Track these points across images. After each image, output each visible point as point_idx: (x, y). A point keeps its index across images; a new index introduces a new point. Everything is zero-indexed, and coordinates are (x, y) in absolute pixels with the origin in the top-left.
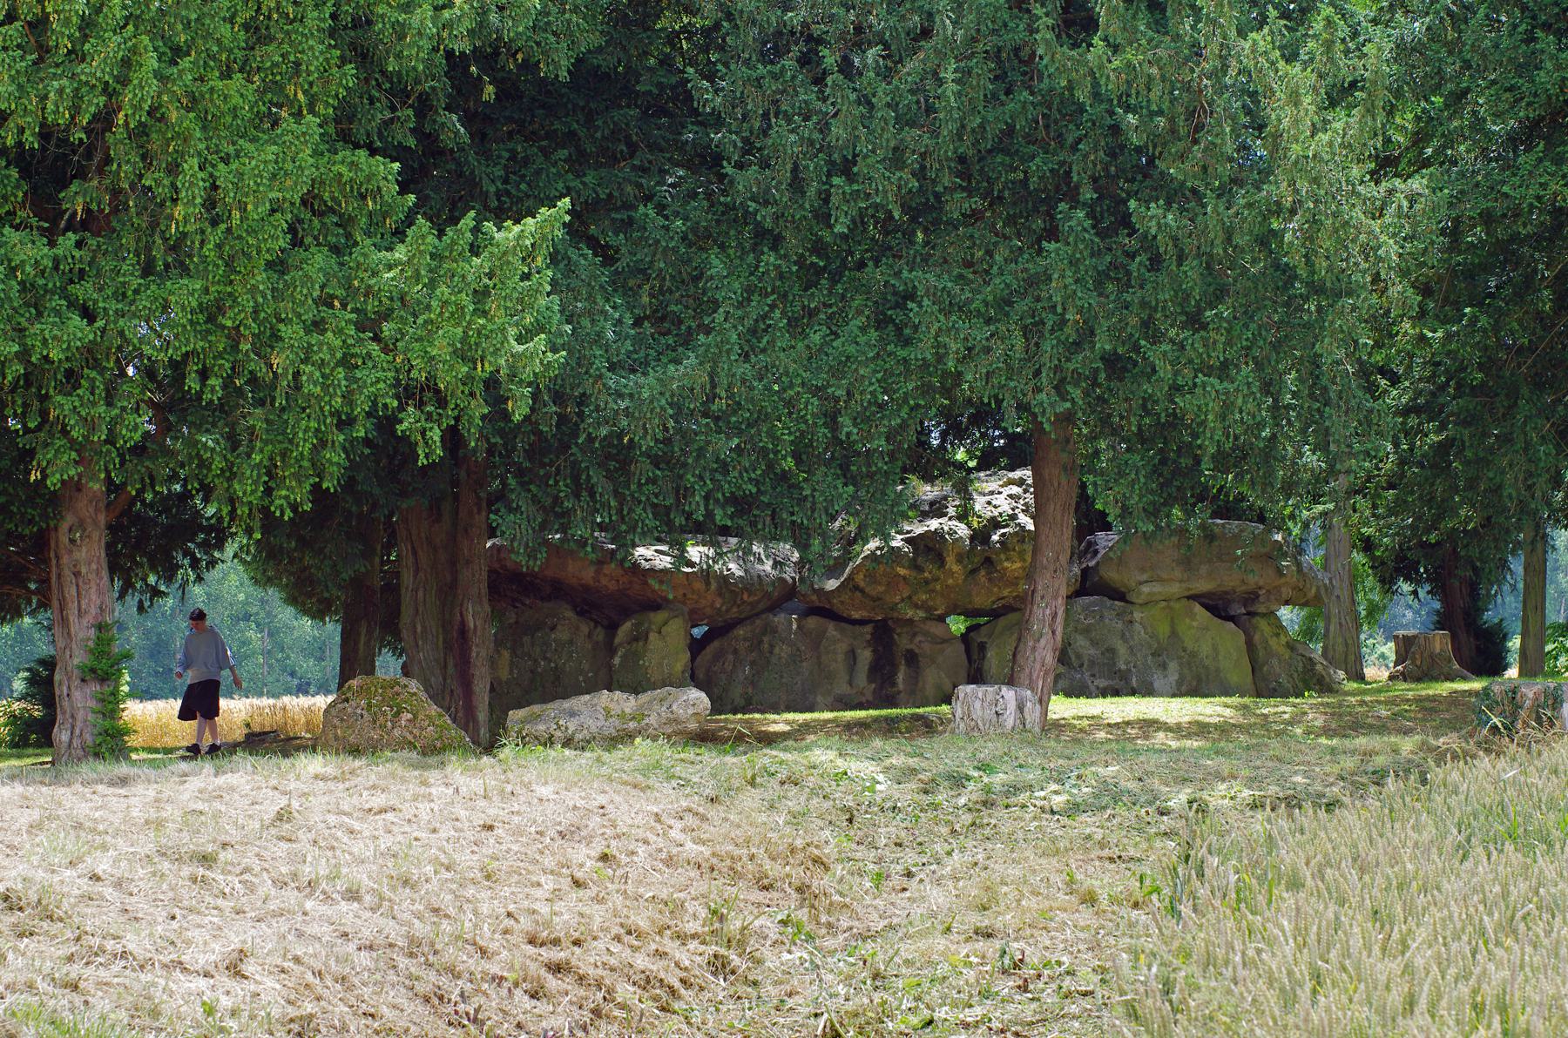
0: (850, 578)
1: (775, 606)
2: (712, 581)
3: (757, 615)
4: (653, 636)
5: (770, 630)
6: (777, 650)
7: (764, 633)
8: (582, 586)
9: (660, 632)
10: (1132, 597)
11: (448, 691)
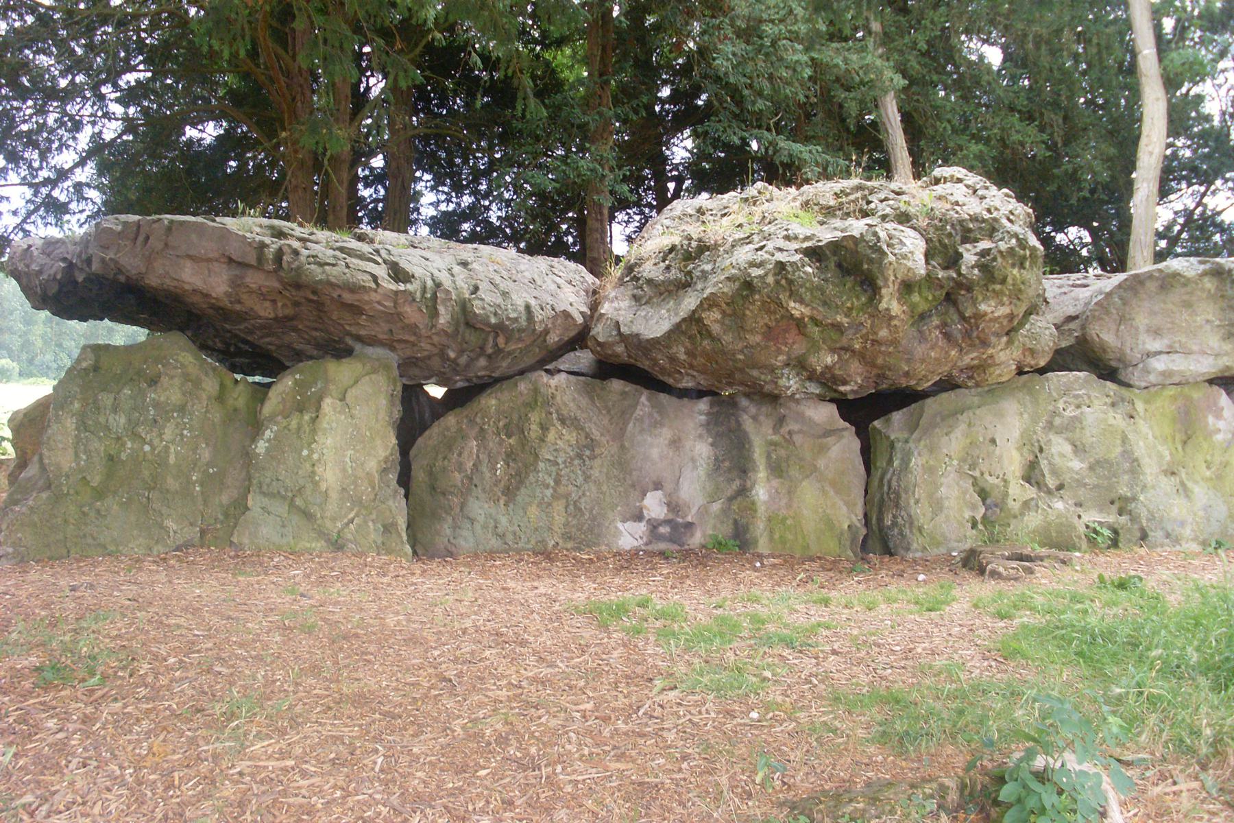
0: (694, 319)
1: (548, 358)
2: (441, 309)
3: (522, 373)
4: (328, 404)
5: (537, 399)
6: (551, 436)
7: (531, 405)
8: (213, 307)
9: (343, 399)
10: (1135, 377)
11: (141, 238)
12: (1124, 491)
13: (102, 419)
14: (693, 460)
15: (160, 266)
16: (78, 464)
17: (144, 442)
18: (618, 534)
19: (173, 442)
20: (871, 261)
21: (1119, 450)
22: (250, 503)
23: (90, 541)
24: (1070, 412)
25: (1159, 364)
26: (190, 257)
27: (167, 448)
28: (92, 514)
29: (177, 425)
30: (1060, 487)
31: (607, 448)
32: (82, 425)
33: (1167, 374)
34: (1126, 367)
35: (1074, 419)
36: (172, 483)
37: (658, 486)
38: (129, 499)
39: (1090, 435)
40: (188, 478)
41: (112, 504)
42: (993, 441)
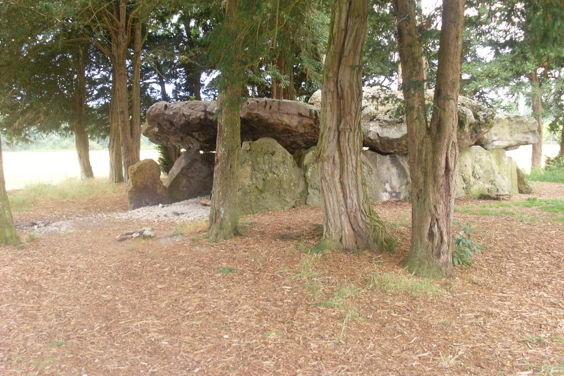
11: (268, 107)
12: (492, 178)
13: (260, 167)
14: (393, 174)
15: (275, 116)
16: (253, 182)
17: (275, 173)
18: (382, 196)
19: (284, 173)
20: (463, 118)
21: (490, 167)
22: (309, 192)
23: (261, 207)
24: (479, 157)
25: (496, 143)
26: (288, 114)
27: (283, 175)
28: (261, 198)
29: (283, 168)
30: (479, 178)
31: (375, 171)
32: (253, 169)
33: (497, 146)
34: (487, 144)
35: (480, 159)
36: (286, 187)
37: (387, 182)
38: (273, 192)
39: (484, 163)
40: (290, 185)
41: (267, 195)
42: (466, 166)
